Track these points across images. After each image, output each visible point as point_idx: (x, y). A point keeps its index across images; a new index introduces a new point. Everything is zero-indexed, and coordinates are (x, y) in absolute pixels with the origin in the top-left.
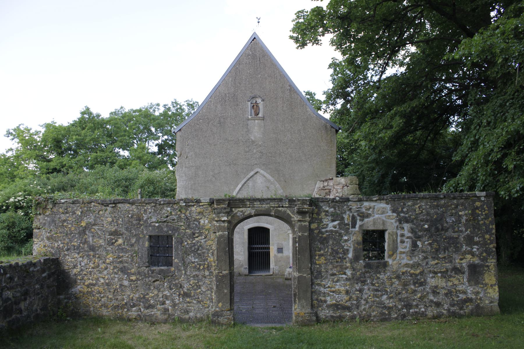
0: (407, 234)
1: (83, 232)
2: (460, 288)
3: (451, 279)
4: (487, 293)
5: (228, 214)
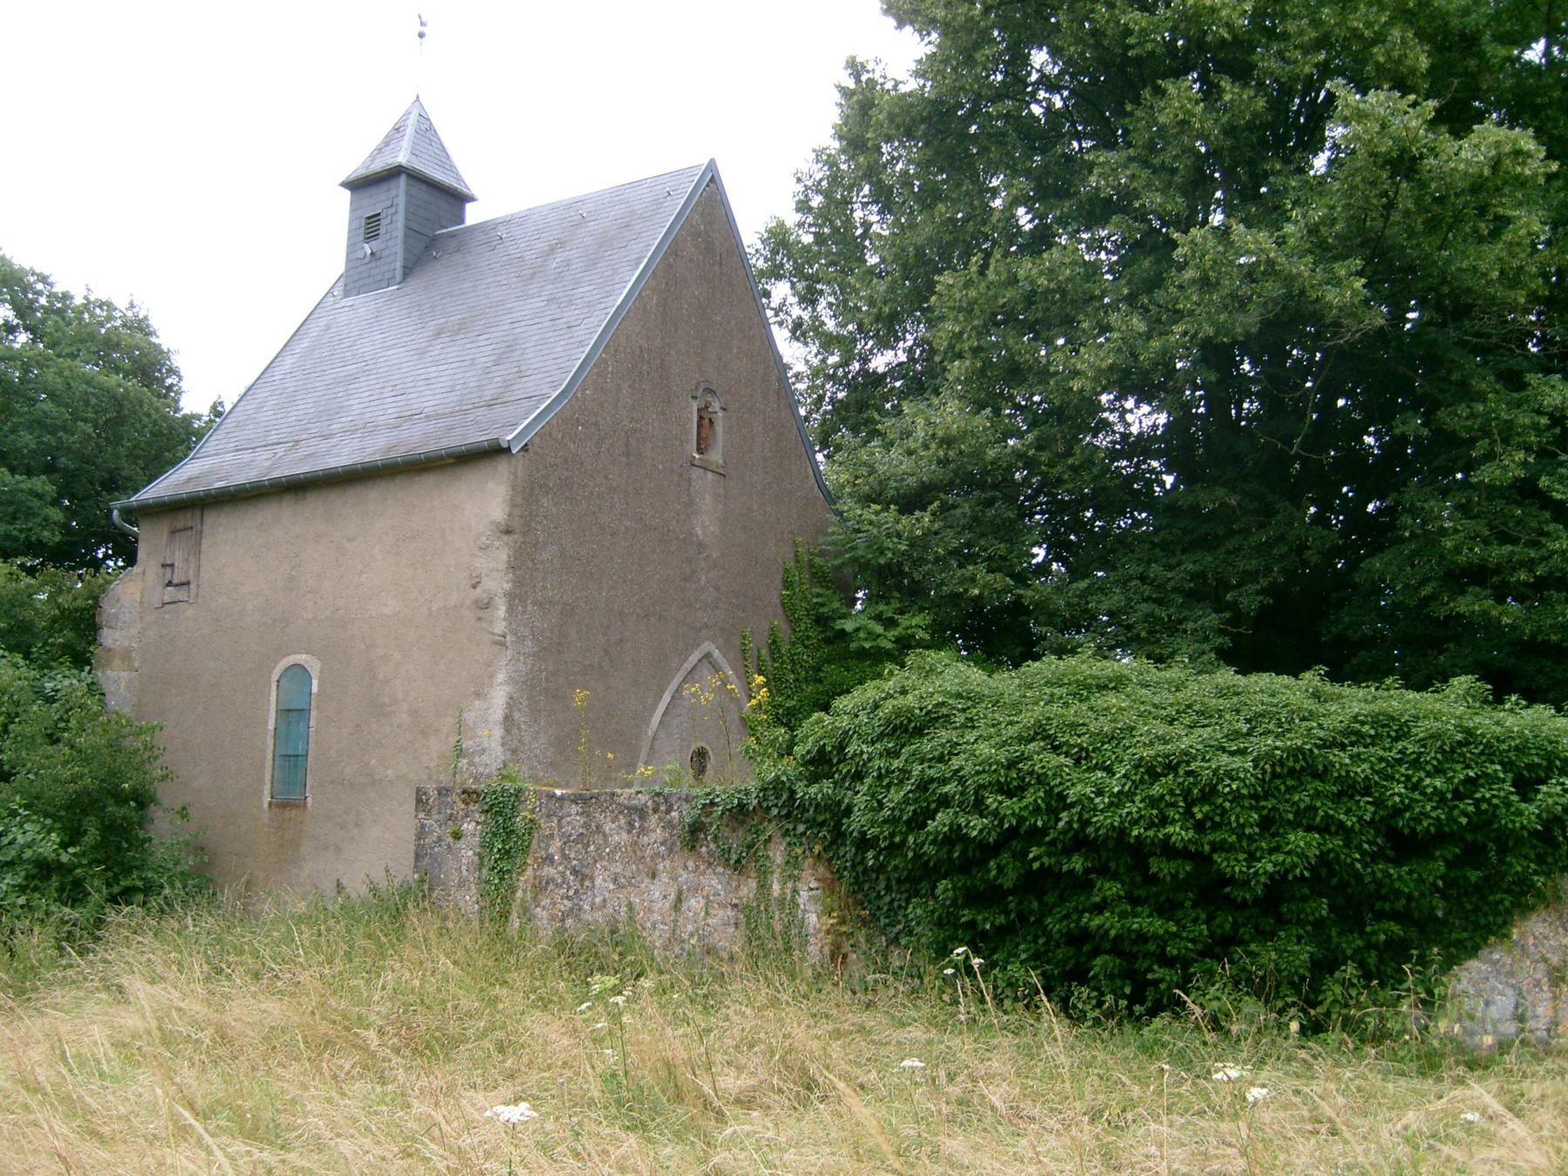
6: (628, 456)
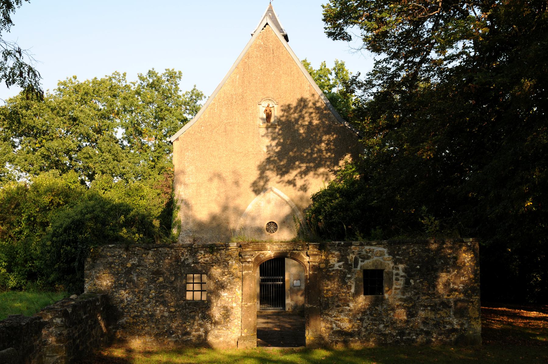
2: (447, 319)
3: (439, 312)
4: (471, 325)
6: (226, 132)
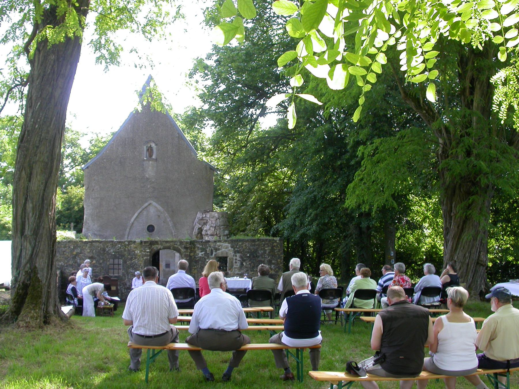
0: (238, 258)
1: (74, 257)
5: (149, 248)
